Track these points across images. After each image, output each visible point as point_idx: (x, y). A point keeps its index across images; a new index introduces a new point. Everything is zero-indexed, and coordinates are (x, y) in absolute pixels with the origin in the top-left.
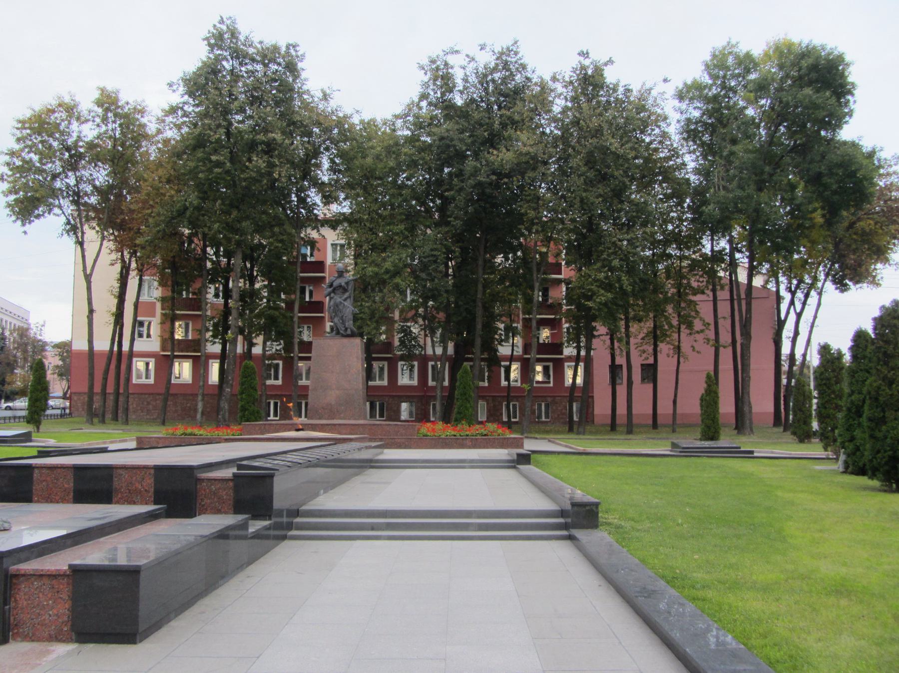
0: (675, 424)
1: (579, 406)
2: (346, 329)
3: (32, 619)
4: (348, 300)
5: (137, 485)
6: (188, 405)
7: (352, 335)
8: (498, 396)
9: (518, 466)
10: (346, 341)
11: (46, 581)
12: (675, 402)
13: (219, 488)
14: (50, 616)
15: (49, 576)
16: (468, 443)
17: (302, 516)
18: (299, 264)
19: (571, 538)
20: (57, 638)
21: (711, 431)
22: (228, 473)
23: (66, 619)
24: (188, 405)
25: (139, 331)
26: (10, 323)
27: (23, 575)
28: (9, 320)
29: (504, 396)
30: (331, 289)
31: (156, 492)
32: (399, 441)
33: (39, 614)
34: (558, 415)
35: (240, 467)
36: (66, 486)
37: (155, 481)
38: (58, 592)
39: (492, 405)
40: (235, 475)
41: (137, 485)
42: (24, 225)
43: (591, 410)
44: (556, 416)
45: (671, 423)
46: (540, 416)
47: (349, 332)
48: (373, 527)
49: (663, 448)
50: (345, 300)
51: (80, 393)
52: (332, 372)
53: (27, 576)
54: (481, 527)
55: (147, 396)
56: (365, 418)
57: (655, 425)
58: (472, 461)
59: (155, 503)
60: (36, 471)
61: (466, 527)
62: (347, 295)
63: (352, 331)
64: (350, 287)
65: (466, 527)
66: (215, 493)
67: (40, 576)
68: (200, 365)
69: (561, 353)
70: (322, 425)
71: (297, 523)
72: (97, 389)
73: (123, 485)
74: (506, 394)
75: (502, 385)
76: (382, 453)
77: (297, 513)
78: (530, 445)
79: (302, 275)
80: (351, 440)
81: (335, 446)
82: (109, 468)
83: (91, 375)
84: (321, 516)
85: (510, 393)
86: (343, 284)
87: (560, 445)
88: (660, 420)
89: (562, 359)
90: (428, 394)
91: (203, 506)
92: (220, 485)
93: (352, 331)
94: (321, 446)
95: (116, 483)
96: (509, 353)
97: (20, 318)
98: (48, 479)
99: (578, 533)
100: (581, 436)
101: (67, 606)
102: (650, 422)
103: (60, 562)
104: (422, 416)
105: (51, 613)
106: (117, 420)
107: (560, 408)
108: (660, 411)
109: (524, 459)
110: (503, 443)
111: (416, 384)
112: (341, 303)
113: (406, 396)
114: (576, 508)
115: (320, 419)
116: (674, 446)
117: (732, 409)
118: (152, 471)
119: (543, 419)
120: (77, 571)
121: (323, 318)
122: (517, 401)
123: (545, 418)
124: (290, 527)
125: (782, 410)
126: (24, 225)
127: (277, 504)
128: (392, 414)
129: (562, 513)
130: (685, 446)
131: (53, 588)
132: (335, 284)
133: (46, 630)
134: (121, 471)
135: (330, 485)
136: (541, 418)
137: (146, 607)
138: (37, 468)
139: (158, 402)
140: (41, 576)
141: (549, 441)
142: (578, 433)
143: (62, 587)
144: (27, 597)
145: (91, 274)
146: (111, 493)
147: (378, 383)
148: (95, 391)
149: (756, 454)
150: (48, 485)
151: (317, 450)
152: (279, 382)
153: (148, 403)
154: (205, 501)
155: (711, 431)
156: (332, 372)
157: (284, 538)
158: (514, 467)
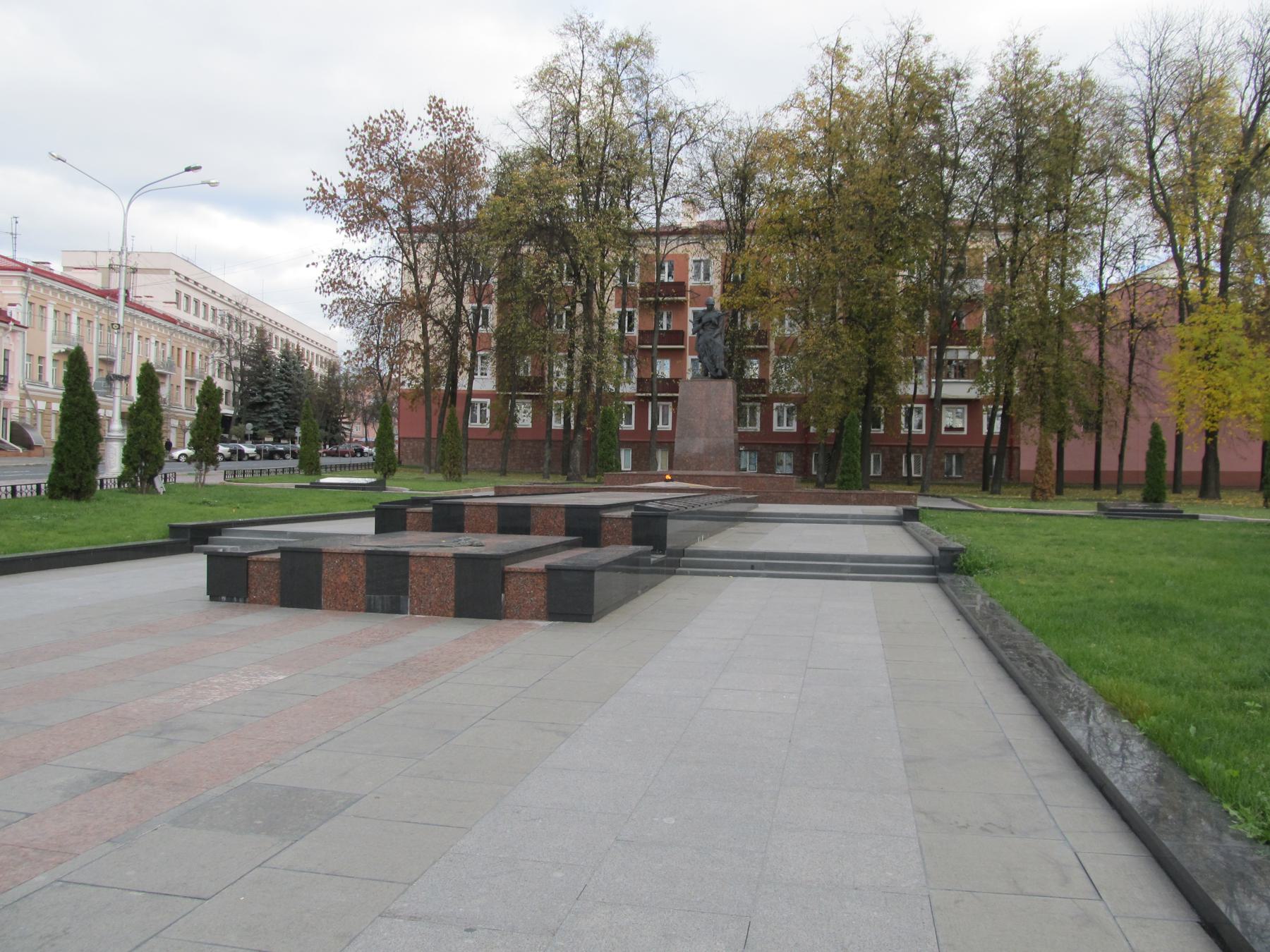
0: (1120, 482)
2: (717, 370)
4: (719, 337)
5: (551, 521)
6: (528, 452)
7: (724, 377)
8: (898, 446)
9: (905, 522)
10: (714, 383)
12: (1121, 457)
16: (853, 498)
17: (687, 556)
19: (936, 581)
20: (536, 617)
21: (1154, 495)
22: (627, 513)
23: (543, 603)
24: (528, 452)
26: (321, 358)
28: (316, 352)
29: (904, 446)
30: (700, 325)
32: (775, 494)
34: (974, 471)
35: (637, 508)
39: (889, 456)
40: (633, 515)
41: (551, 521)
43: (1015, 464)
44: (970, 471)
45: (1116, 483)
46: (950, 472)
47: (720, 373)
48: (752, 567)
49: (1090, 509)
50: (715, 337)
51: (409, 439)
53: (515, 573)
54: (854, 570)
55: (482, 442)
57: (1097, 485)
58: (854, 516)
59: (567, 535)
61: (839, 569)
62: (718, 331)
63: (723, 372)
65: (839, 569)
67: (524, 573)
68: (542, 407)
70: (690, 476)
71: (683, 561)
72: (434, 435)
74: (906, 444)
75: (774, 430)
76: (757, 507)
77: (683, 553)
78: (921, 503)
80: (725, 491)
81: (707, 497)
82: (527, 507)
84: (704, 557)
85: (910, 443)
86: (713, 319)
88: (1103, 481)
90: (809, 443)
93: (723, 372)
94: (694, 496)
95: (533, 520)
96: (911, 392)
97: (319, 346)
98: (477, 515)
99: (942, 576)
100: (996, 496)
102: (1092, 481)
103: (539, 563)
104: (802, 471)
107: (975, 462)
108: (1103, 467)
109: (912, 515)
110: (892, 500)
111: (795, 431)
112: (711, 340)
113: (783, 445)
115: (687, 470)
116: (1100, 507)
117: (1198, 467)
118: (563, 510)
119: (954, 475)
120: (550, 569)
122: (921, 452)
123: (956, 474)
124: (677, 564)
127: (669, 545)
128: (766, 466)
129: (932, 560)
130: (1112, 508)
132: (704, 320)
135: (710, 534)
136: (951, 474)
137: (599, 597)
139: (494, 449)
140: (525, 573)
142: (993, 493)
147: (749, 429)
148: (433, 436)
149: (1184, 513)
151: (696, 499)
152: (632, 427)
153: (483, 451)
155: (1154, 495)
157: (674, 573)
158: (900, 524)
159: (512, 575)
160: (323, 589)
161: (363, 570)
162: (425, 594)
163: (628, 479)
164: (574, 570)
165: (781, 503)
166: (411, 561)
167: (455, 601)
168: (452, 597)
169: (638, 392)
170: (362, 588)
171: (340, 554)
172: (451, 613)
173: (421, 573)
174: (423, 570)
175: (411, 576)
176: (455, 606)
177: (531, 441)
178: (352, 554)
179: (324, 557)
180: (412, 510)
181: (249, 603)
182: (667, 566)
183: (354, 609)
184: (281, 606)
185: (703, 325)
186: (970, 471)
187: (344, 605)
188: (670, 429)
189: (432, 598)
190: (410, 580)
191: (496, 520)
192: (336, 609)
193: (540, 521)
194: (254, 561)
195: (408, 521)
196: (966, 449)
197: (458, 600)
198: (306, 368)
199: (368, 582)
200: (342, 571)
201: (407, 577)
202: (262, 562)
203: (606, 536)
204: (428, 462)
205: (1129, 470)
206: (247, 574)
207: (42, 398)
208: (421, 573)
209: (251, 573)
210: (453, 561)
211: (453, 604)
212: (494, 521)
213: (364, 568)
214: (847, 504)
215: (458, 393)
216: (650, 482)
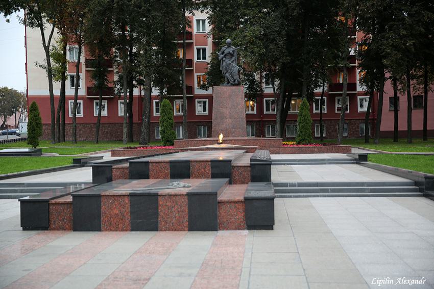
2: (235, 81)
5: (202, 170)
7: (239, 84)
10: (234, 88)
11: (232, 204)
15: (234, 202)
16: (316, 150)
18: (185, 35)
20: (239, 228)
23: (242, 220)
27: (223, 202)
30: (223, 55)
33: (231, 219)
34: (353, 132)
42: (5, 16)
44: (352, 133)
47: (236, 82)
50: (232, 62)
52: (227, 107)
56: (248, 135)
58: (329, 160)
60: (150, 164)
64: (235, 54)
69: (356, 90)
73: (196, 170)
75: (264, 113)
83: (53, 112)
86: (231, 52)
87: (367, 150)
89: (356, 93)
91: (235, 180)
92: (243, 169)
98: (157, 168)
106: (64, 141)
114: (427, 180)
119: (266, 136)
121: (192, 70)
125: (176, 96)
126: (5, 16)
132: (226, 52)
134: (194, 163)
138: (151, 163)
141: (359, 148)
145: (49, 46)
150: (157, 171)
156: (227, 107)
159: (222, 204)
161: (128, 205)
162: (169, 218)
164: (259, 199)
165: (276, 154)
166: (160, 199)
168: (186, 219)
169: (88, 95)
171: (114, 196)
172: (186, 229)
173: (166, 206)
175: (160, 208)
176: (189, 224)
177: (108, 124)
178: (120, 196)
179: (102, 199)
180: (115, 166)
181: (50, 230)
182: (331, 192)
183: (123, 230)
184: (74, 231)
185: (225, 55)
186: (352, 133)
187: (116, 226)
189: (174, 220)
190: (159, 210)
191: (169, 171)
192: (111, 230)
193: (196, 170)
194: (53, 204)
195: (113, 174)
196: (348, 121)
199: (131, 213)
200: (115, 206)
201: (157, 208)
202: (58, 204)
203: (235, 177)
204: (54, 137)
205: (401, 130)
206: (49, 212)
208: (166, 206)
209: (51, 212)
210: (186, 197)
211: (187, 223)
212: (208, 169)
213: (129, 204)
214: (313, 153)
216: (210, 144)
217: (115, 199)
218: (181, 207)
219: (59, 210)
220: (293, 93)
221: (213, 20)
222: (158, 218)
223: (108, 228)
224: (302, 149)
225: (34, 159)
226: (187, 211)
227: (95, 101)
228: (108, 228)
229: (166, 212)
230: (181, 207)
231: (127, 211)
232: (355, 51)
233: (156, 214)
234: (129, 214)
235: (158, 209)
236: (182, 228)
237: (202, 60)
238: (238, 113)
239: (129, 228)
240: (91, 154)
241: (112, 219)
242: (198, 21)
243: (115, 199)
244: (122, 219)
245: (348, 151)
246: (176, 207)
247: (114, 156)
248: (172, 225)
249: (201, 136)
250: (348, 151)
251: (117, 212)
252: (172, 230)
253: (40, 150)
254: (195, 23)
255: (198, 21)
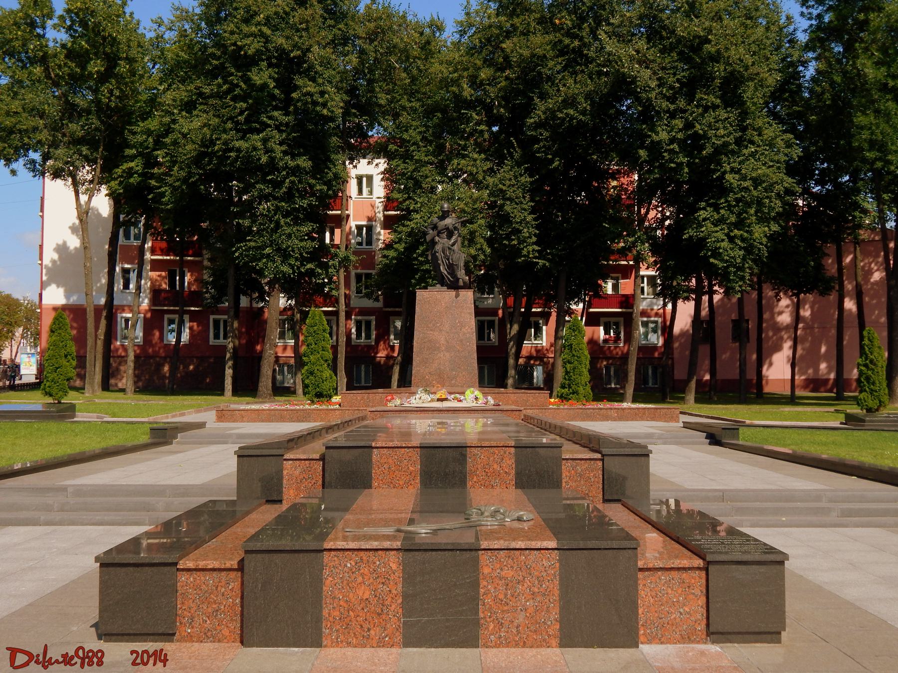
1: (153, 531)
3: (662, 618)
5: (495, 466)
11: (675, 574)
13: (586, 469)
14: (681, 614)
25: (349, 289)
31: (518, 475)
36: (411, 468)
37: (516, 461)
38: (689, 587)
41: (495, 466)
66: (581, 476)
75: (211, 343)
79: (401, 309)
98: (390, 461)
101: (700, 603)
105: (682, 610)
131: (684, 582)
133: (677, 630)
143: (693, 581)
144: (654, 594)
146: (465, 477)
154: (571, 484)
160: (325, 612)
162: (508, 611)
163: (644, 414)
167: (561, 621)
168: (555, 614)
170: (395, 607)
172: (554, 642)
174: (503, 573)
175: (483, 583)
176: (561, 629)
188: (177, 316)
189: (521, 618)
192: (349, 644)
197: (564, 620)
198: (537, 248)
199: (405, 596)
200: (360, 579)
201: (476, 585)
207: (338, 278)
215: (241, 309)
216: (583, 420)
217: (361, 559)
218: (541, 583)
219: (204, 587)
220: (534, 310)
221: (389, 175)
222: (477, 613)
223: (342, 637)
224: (588, 411)
225: (53, 425)
226: (557, 592)
227: (166, 317)
228: (342, 637)
229: (502, 596)
230: (541, 583)
231: (394, 592)
232: (662, 234)
233: (474, 600)
234: (400, 601)
235: (479, 585)
236: (544, 640)
237: (364, 246)
238: (461, 341)
239: (399, 638)
240: (173, 417)
241: (351, 613)
242: (360, 179)
243: (361, 559)
244: (379, 614)
245: (672, 417)
246: (527, 583)
247: (223, 422)
248: (514, 631)
249: (360, 383)
250: (672, 417)
251: (366, 596)
252: (517, 645)
253: (72, 408)
254: (353, 184)
255: (360, 179)
